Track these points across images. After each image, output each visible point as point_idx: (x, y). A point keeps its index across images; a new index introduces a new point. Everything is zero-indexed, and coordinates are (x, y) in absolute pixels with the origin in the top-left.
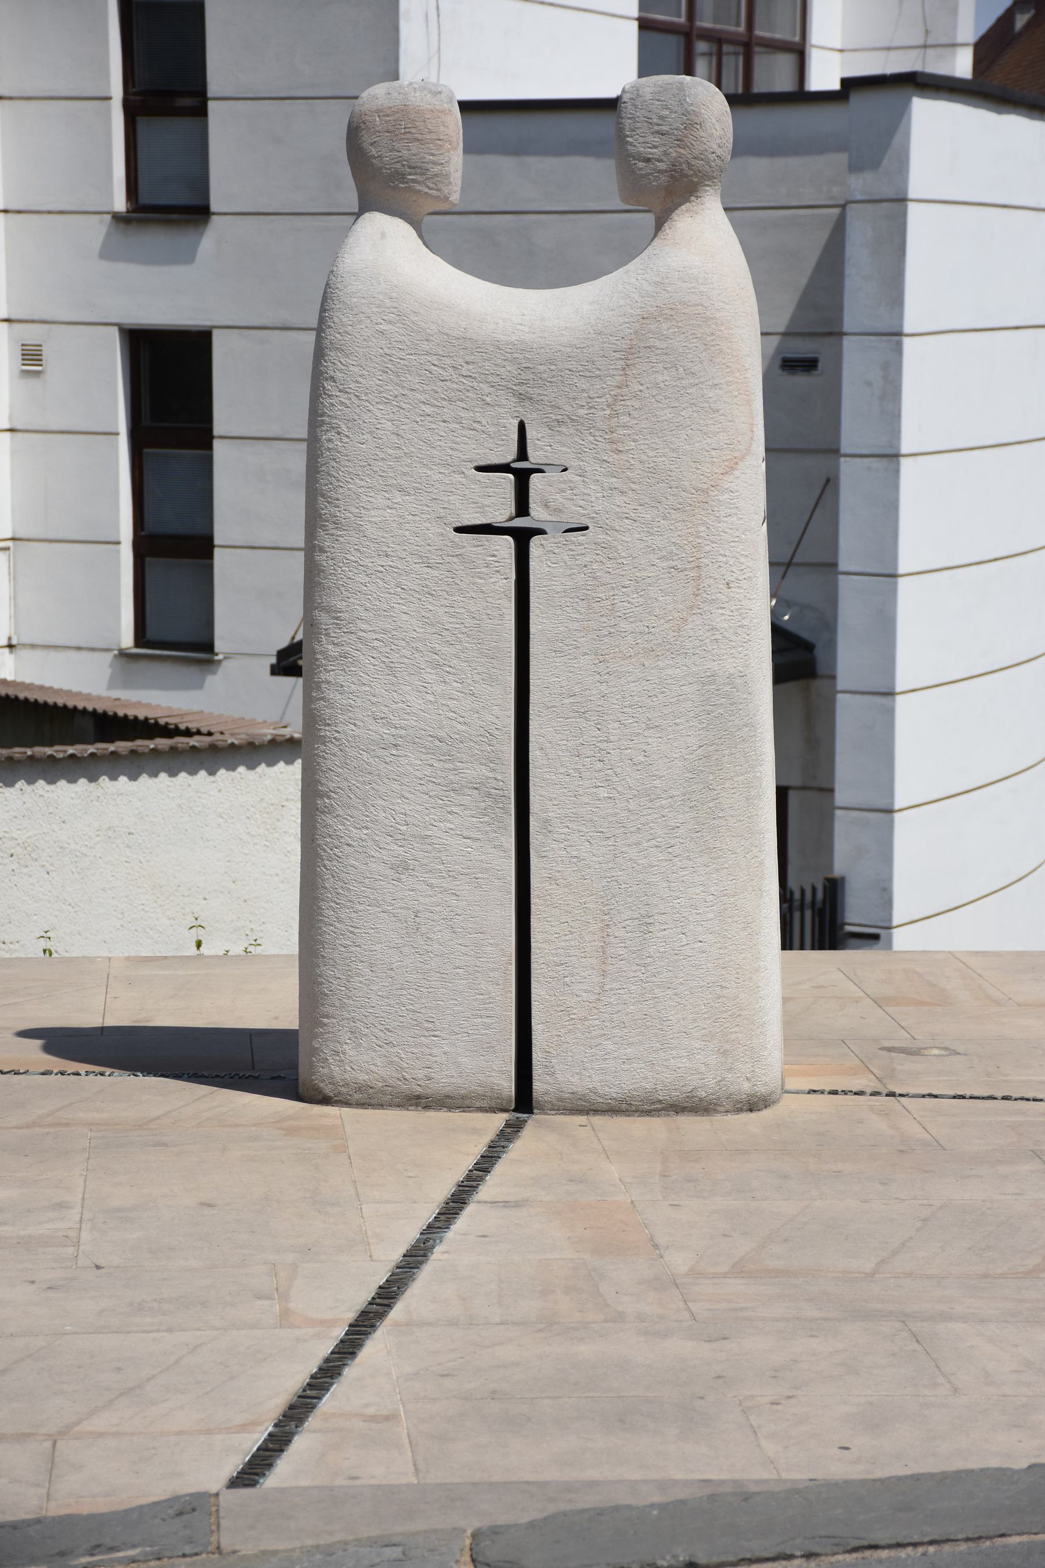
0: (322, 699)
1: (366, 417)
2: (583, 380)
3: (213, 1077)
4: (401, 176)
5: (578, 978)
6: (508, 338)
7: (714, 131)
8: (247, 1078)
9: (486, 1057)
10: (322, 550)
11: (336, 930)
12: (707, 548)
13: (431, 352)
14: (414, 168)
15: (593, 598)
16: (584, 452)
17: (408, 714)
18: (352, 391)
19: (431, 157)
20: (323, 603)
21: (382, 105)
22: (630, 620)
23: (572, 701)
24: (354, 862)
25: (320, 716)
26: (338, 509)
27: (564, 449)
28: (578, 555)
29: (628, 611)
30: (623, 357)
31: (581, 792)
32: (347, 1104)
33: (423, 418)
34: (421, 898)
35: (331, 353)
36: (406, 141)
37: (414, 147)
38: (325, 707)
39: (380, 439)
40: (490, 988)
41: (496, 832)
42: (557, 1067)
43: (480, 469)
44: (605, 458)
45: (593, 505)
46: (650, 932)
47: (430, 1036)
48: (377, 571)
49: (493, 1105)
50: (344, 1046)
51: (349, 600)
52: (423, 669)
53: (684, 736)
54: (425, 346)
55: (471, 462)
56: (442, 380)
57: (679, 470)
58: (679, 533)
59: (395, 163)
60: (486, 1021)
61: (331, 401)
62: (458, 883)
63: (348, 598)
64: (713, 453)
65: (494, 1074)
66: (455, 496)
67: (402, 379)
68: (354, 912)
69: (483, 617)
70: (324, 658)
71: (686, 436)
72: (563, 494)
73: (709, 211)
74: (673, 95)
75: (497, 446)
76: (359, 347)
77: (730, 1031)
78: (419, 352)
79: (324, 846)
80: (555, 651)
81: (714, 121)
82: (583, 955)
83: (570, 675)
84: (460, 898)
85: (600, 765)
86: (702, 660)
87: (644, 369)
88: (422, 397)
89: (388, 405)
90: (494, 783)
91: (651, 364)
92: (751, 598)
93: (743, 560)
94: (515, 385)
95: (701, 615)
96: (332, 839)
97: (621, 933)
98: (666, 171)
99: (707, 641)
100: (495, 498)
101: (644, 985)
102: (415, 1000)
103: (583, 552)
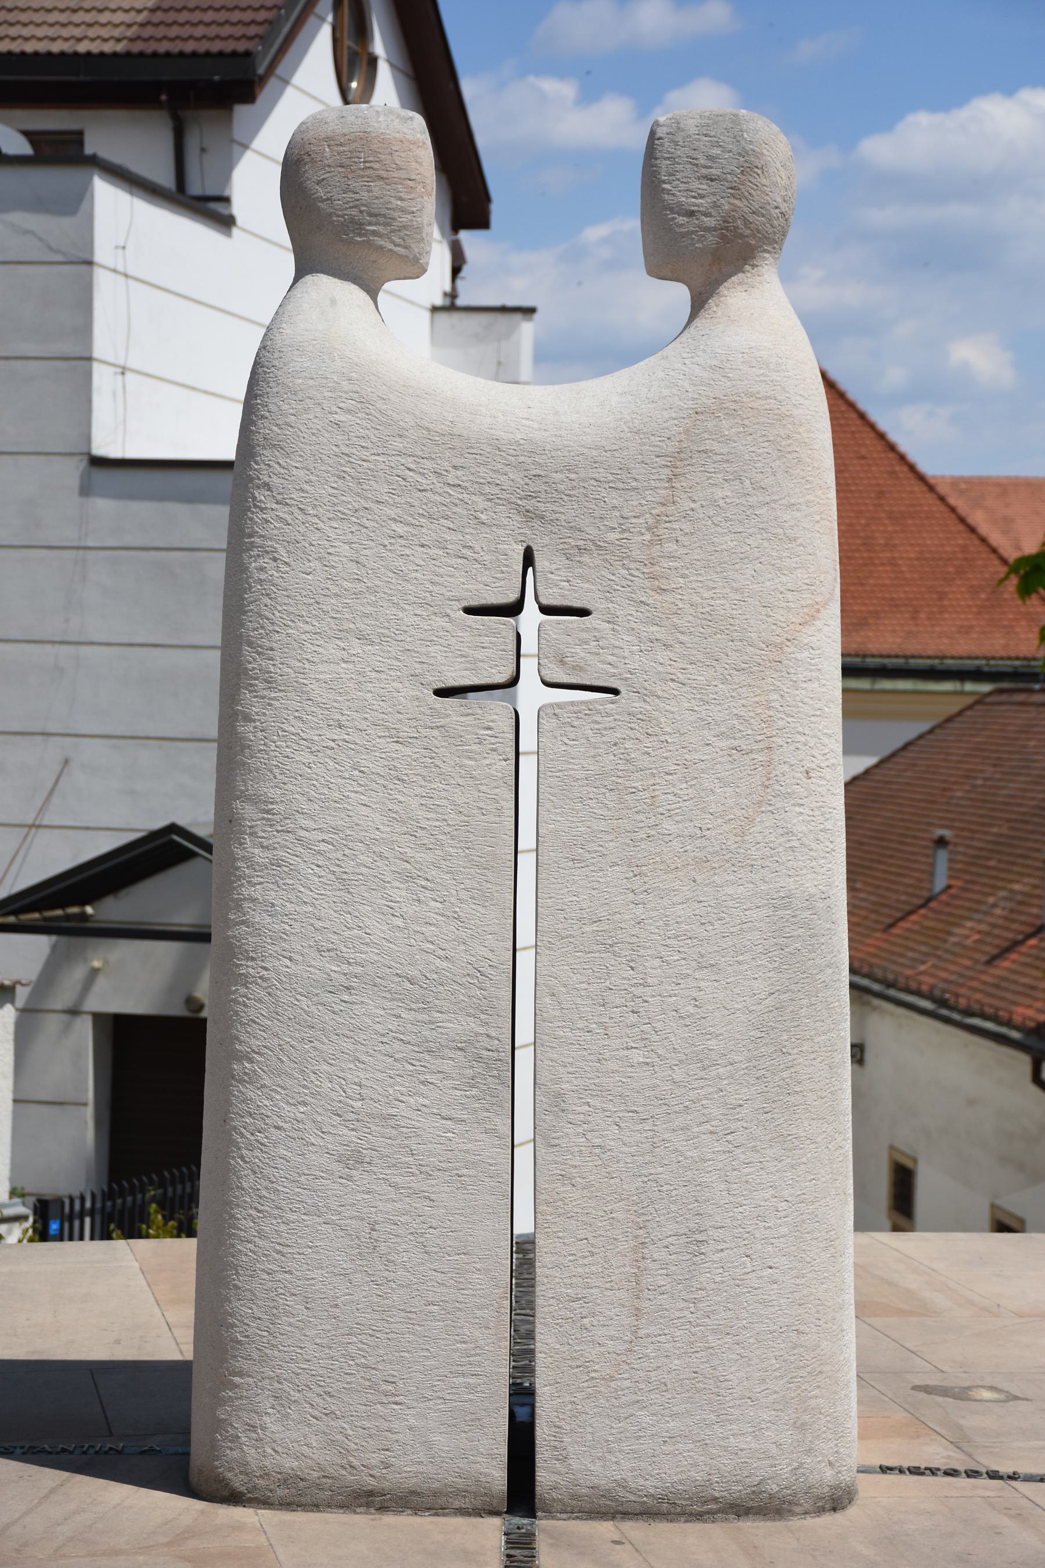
0: (243, 922)
1: (314, 537)
2: (614, 494)
3: (58, 1453)
4: (358, 226)
5: (601, 1318)
6: (511, 436)
7: (779, 179)
8: (106, 1453)
9: (470, 1434)
10: (248, 719)
11: (256, 1250)
12: (781, 723)
13: (406, 452)
14: (376, 215)
15: (626, 788)
16: (615, 590)
17: (367, 944)
18: (295, 503)
19: (399, 203)
20: (247, 790)
21: (333, 131)
22: (677, 819)
23: (595, 928)
24: (285, 1153)
25: (240, 947)
26: (271, 662)
27: (587, 585)
28: (605, 729)
29: (673, 806)
30: (669, 464)
31: (607, 1056)
32: (265, 1503)
33: (393, 541)
34: (379, 1203)
35: (265, 452)
36: (367, 179)
37: (377, 187)
38: (247, 933)
39: (333, 567)
40: (477, 1333)
41: (487, 1110)
42: (570, 1449)
43: (470, 611)
44: (643, 599)
45: (627, 662)
46: (702, 1253)
47: (389, 1403)
48: (327, 747)
49: (478, 1504)
50: (264, 1418)
51: (286, 787)
52: (389, 882)
53: (749, 980)
54: (398, 444)
55: (458, 600)
56: (420, 490)
57: (745, 617)
58: (743, 702)
59: (352, 207)
60: (471, 1381)
61: (264, 516)
62: (433, 1182)
63: (285, 784)
64: (789, 596)
65: (480, 1459)
66: (436, 647)
67: (365, 487)
68: (283, 1223)
69: (474, 812)
70: (248, 867)
71: (753, 572)
72: (585, 647)
73: (768, 285)
74: (726, 129)
75: (495, 580)
76: (306, 444)
77: (809, 1395)
78: (389, 452)
79: (243, 1130)
80: (573, 860)
81: (778, 165)
82: (608, 1286)
83: (594, 892)
84: (436, 1203)
85: (633, 1018)
86: (773, 875)
87: (698, 481)
88: (392, 513)
89: (345, 523)
90: (485, 1042)
91: (707, 474)
92: (835, 792)
93: (826, 740)
94: (520, 499)
95: (773, 813)
96: (254, 1118)
97: (661, 1255)
98: (715, 229)
99: (781, 849)
100: (491, 651)
101: (693, 1330)
102: (369, 1350)
103: (613, 725)
